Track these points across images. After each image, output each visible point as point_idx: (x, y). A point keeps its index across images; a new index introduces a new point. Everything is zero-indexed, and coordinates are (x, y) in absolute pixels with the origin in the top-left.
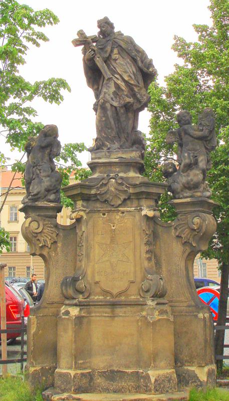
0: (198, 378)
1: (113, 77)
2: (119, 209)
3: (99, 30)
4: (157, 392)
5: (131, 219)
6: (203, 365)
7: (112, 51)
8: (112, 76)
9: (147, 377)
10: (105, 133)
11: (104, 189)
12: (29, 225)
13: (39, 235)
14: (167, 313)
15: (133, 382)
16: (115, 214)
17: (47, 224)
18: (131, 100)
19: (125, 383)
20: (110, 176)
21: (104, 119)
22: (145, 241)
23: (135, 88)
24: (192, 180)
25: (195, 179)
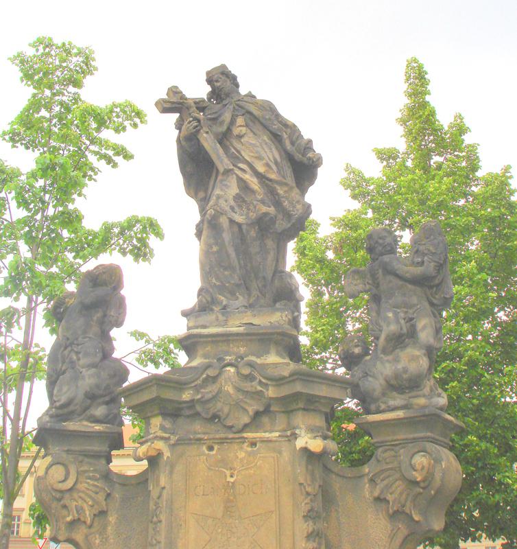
1: (235, 168)
2: (245, 435)
7: (233, 122)
8: (231, 167)
10: (217, 278)
11: (210, 391)
13: (67, 495)
16: (236, 446)
21: (215, 249)
22: (304, 508)
23: (278, 187)
24: (405, 370)
25: (413, 368)
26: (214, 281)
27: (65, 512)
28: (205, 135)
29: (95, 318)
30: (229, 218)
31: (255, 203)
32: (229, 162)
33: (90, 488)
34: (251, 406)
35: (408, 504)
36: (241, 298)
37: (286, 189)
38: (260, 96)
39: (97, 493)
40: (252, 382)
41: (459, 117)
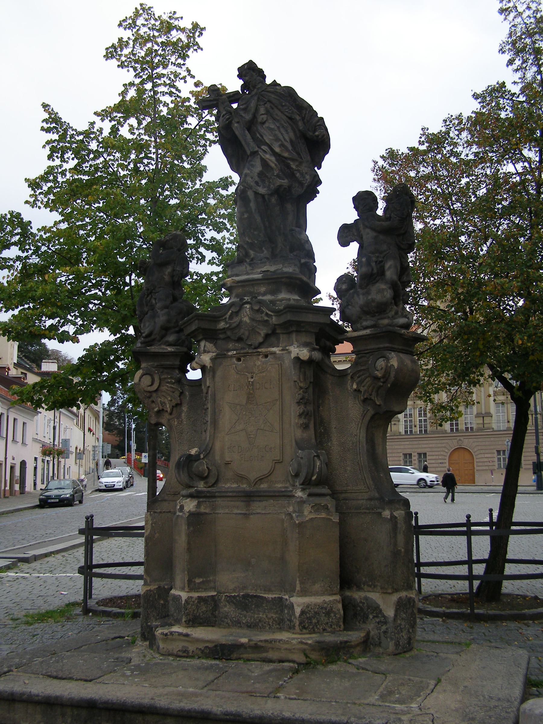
0: (381, 610)
1: (260, 150)
2: (260, 350)
3: (241, 82)
4: (304, 631)
5: (277, 366)
6: (390, 591)
7: (257, 110)
8: (257, 149)
9: (291, 607)
12: (140, 380)
14: (327, 508)
15: (276, 613)
16: (255, 358)
17: (165, 378)
18: (285, 182)
19: (263, 615)
20: (245, 299)
22: (298, 397)
23: (291, 163)
25: (378, 298)
26: (247, 239)
27: (154, 405)
28: (236, 125)
29: (167, 273)
30: (254, 191)
31: (273, 177)
32: (254, 145)
33: (169, 389)
34: (263, 330)
35: (374, 393)
36: (265, 252)
37: (297, 163)
38: (283, 83)
39: (173, 392)
40: (262, 314)
41: (507, 66)
